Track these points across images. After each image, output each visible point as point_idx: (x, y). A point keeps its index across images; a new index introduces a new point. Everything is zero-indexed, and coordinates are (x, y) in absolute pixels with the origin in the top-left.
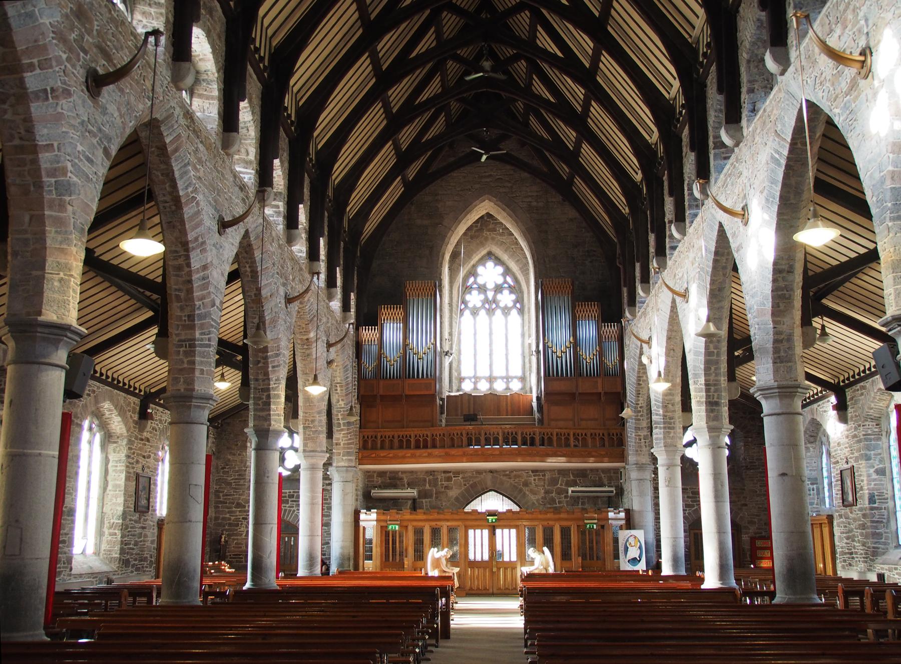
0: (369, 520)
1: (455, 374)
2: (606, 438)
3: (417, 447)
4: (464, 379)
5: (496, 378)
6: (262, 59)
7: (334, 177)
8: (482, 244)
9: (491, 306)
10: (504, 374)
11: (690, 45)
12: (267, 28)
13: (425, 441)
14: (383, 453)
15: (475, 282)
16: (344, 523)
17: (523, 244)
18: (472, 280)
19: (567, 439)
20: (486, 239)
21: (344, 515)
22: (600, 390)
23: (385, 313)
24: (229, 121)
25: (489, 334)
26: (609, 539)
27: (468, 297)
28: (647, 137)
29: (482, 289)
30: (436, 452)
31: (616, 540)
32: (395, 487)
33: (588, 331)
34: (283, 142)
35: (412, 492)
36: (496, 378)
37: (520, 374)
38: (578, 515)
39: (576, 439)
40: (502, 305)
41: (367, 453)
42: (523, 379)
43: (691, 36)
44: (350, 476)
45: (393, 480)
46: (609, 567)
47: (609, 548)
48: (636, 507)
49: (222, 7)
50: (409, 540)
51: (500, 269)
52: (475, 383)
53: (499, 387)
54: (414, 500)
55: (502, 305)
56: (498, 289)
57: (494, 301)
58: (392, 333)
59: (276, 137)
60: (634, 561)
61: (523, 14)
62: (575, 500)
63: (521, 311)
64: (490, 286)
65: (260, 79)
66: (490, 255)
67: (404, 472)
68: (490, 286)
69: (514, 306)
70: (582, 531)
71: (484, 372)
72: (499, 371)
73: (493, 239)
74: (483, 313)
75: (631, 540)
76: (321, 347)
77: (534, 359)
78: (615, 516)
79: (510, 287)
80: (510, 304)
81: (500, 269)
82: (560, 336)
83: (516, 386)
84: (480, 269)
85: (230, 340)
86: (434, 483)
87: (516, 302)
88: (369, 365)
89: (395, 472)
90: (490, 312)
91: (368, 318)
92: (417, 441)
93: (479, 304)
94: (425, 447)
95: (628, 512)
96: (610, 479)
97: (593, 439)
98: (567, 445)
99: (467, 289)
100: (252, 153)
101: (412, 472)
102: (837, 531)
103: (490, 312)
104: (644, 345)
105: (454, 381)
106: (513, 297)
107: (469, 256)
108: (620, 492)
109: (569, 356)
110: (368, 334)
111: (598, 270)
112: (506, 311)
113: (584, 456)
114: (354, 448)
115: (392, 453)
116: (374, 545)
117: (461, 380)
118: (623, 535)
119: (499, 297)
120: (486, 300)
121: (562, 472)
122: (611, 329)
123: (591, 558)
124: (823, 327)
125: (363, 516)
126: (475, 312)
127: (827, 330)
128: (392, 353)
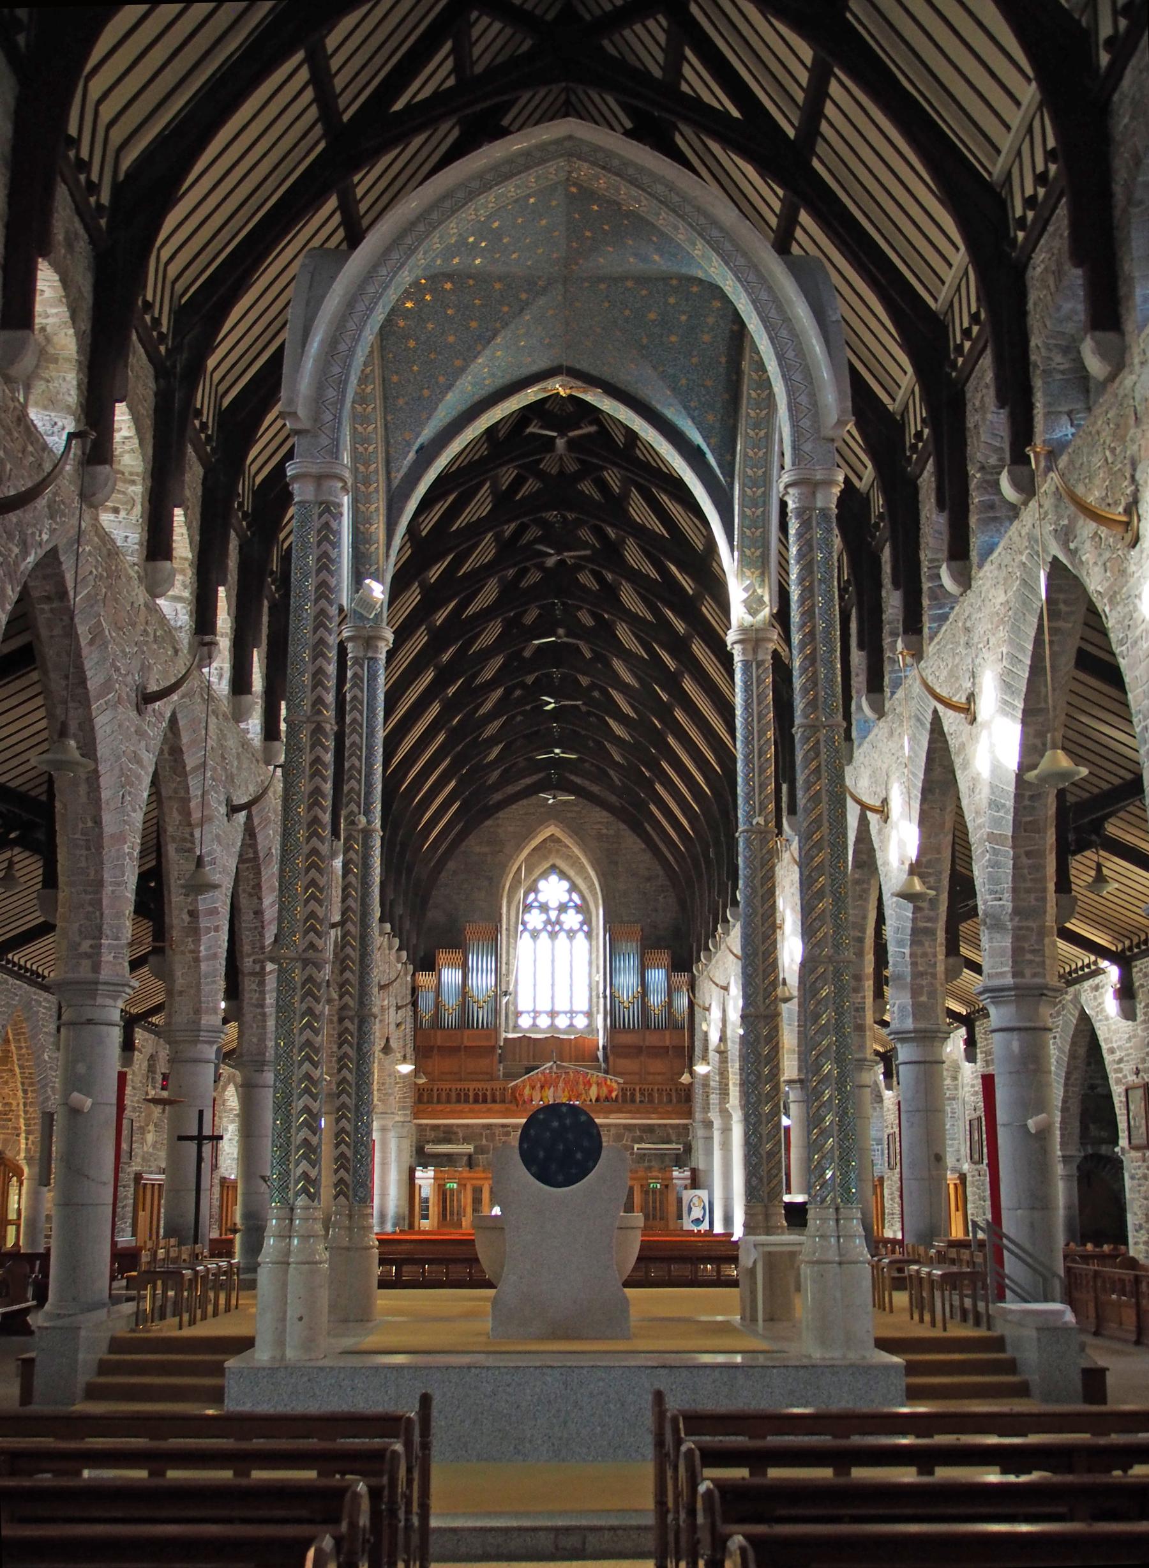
0: (425, 1178)
1: (512, 1008)
2: (674, 1094)
3: (476, 1101)
4: (521, 1013)
5: (558, 1013)
6: (162, 337)
7: (97, 87)
8: (546, 858)
9: (553, 928)
10: (567, 1009)
11: (933, 315)
12: (100, 102)
13: (485, 1095)
14: (440, 1107)
15: (536, 900)
16: (399, 1181)
17: (592, 874)
18: (532, 896)
19: (633, 1095)
20: (550, 852)
21: (399, 1172)
22: (667, 1043)
23: (442, 956)
24: (157, 545)
25: (552, 966)
26: (672, 1198)
27: (527, 917)
28: (886, 399)
29: (544, 908)
30: (497, 1107)
31: (680, 1201)
32: (448, 1141)
33: (657, 977)
34: (139, 370)
35: (469, 1148)
36: (558, 1013)
37: (586, 1008)
38: (641, 1174)
39: (642, 1094)
40: (566, 927)
41: (422, 1107)
42: (589, 1014)
43: (990, 174)
44: (404, 1132)
45: (448, 1135)
46: (672, 1226)
47: (673, 1209)
48: (701, 1166)
49: (146, 352)
50: (467, 1198)
51: (565, 885)
52: (534, 1018)
53: (562, 1022)
54: (470, 1156)
55: (566, 927)
56: (563, 908)
57: (558, 922)
58: (451, 977)
59: (123, 350)
60: (698, 1221)
61: (651, 23)
62: (642, 1157)
63: (589, 935)
64: (553, 904)
65: (152, 357)
66: (554, 868)
67: (458, 1126)
68: (553, 904)
69: (581, 929)
70: (646, 1191)
71: (544, 1005)
72: (562, 1005)
73: (558, 851)
74: (544, 936)
75: (695, 1200)
76: (392, 1010)
77: (602, 1000)
78: (679, 1175)
79: (576, 906)
80: (576, 926)
81: (565, 885)
82: (628, 981)
83: (581, 1022)
84: (542, 884)
85: (12, 785)
86: (491, 1137)
87: (582, 923)
88: (426, 1016)
89: (452, 1126)
90: (553, 935)
91: (427, 964)
92: (476, 1095)
93: (540, 926)
94: (485, 1101)
95: (694, 1171)
96: (679, 1135)
97: (660, 1094)
98: (633, 1101)
99: (528, 908)
100: (66, 381)
101: (467, 1126)
102: (886, 1192)
103: (553, 935)
104: (872, 817)
105: (511, 1016)
106: (580, 917)
107: (529, 871)
108: (688, 1149)
109: (636, 1008)
110: (424, 979)
111: (672, 907)
112: (571, 934)
113: (647, 1114)
114: (409, 1102)
115: (449, 1107)
116: (430, 1204)
117: (518, 1014)
118: (687, 1195)
119: (563, 917)
120: (548, 922)
121: (627, 1127)
122: (682, 978)
123: (654, 1218)
124: (1099, 867)
125: (418, 1174)
126: (535, 935)
127: (1105, 871)
128: (451, 1001)
